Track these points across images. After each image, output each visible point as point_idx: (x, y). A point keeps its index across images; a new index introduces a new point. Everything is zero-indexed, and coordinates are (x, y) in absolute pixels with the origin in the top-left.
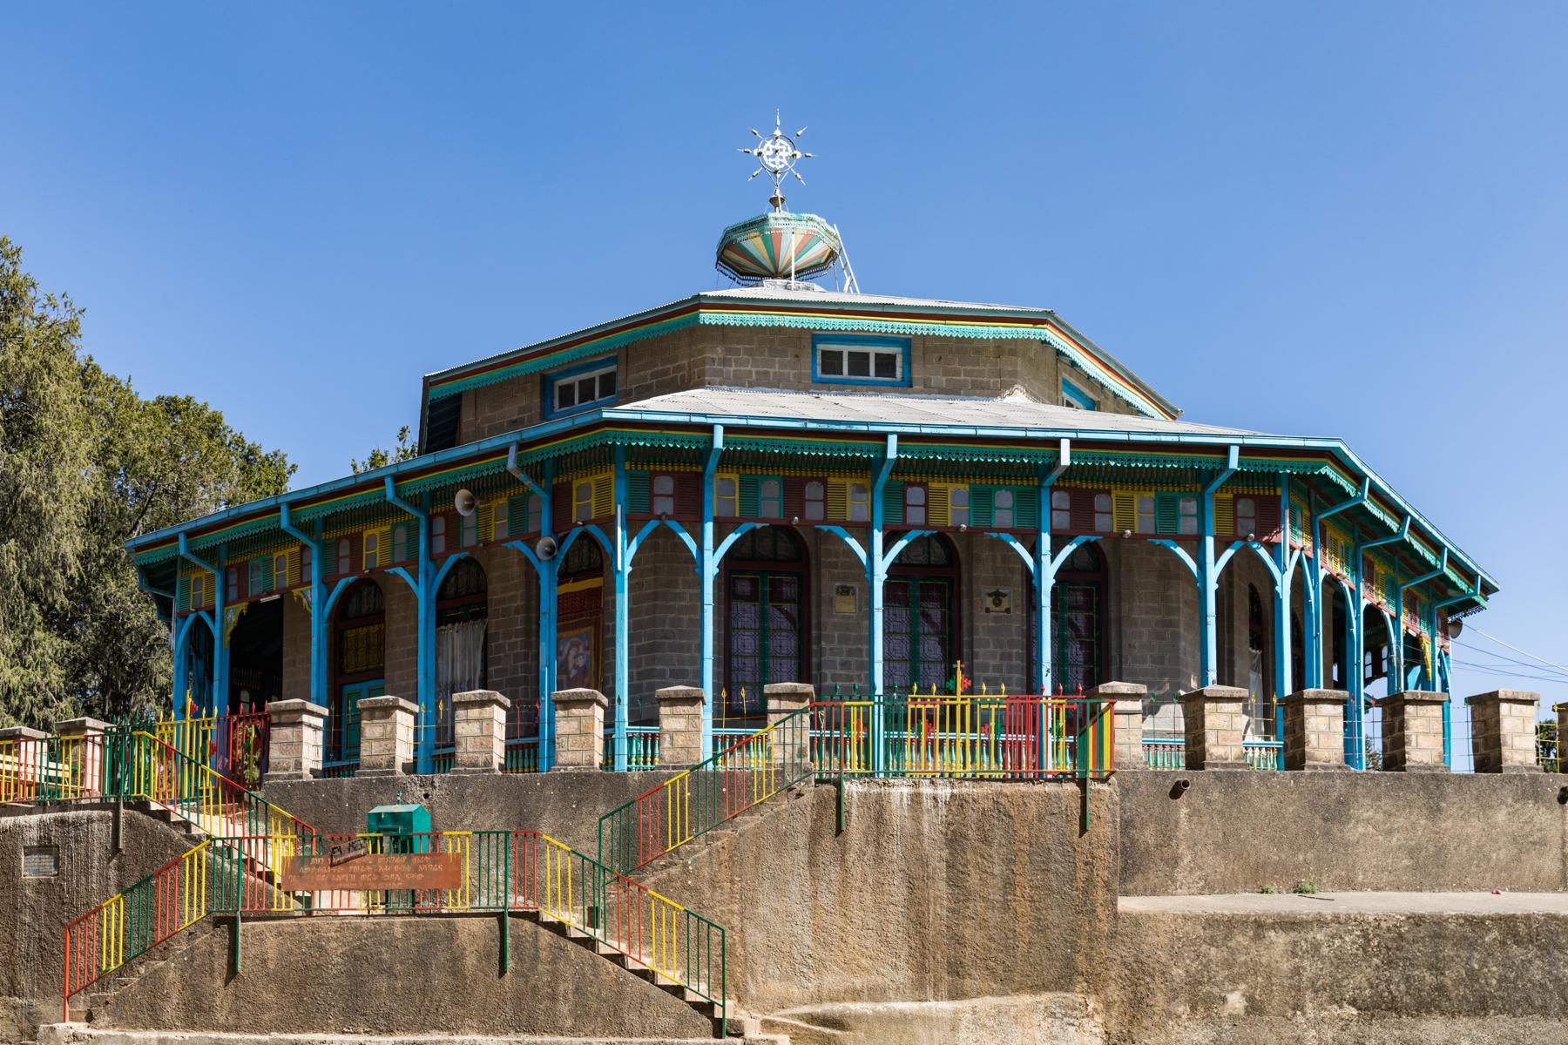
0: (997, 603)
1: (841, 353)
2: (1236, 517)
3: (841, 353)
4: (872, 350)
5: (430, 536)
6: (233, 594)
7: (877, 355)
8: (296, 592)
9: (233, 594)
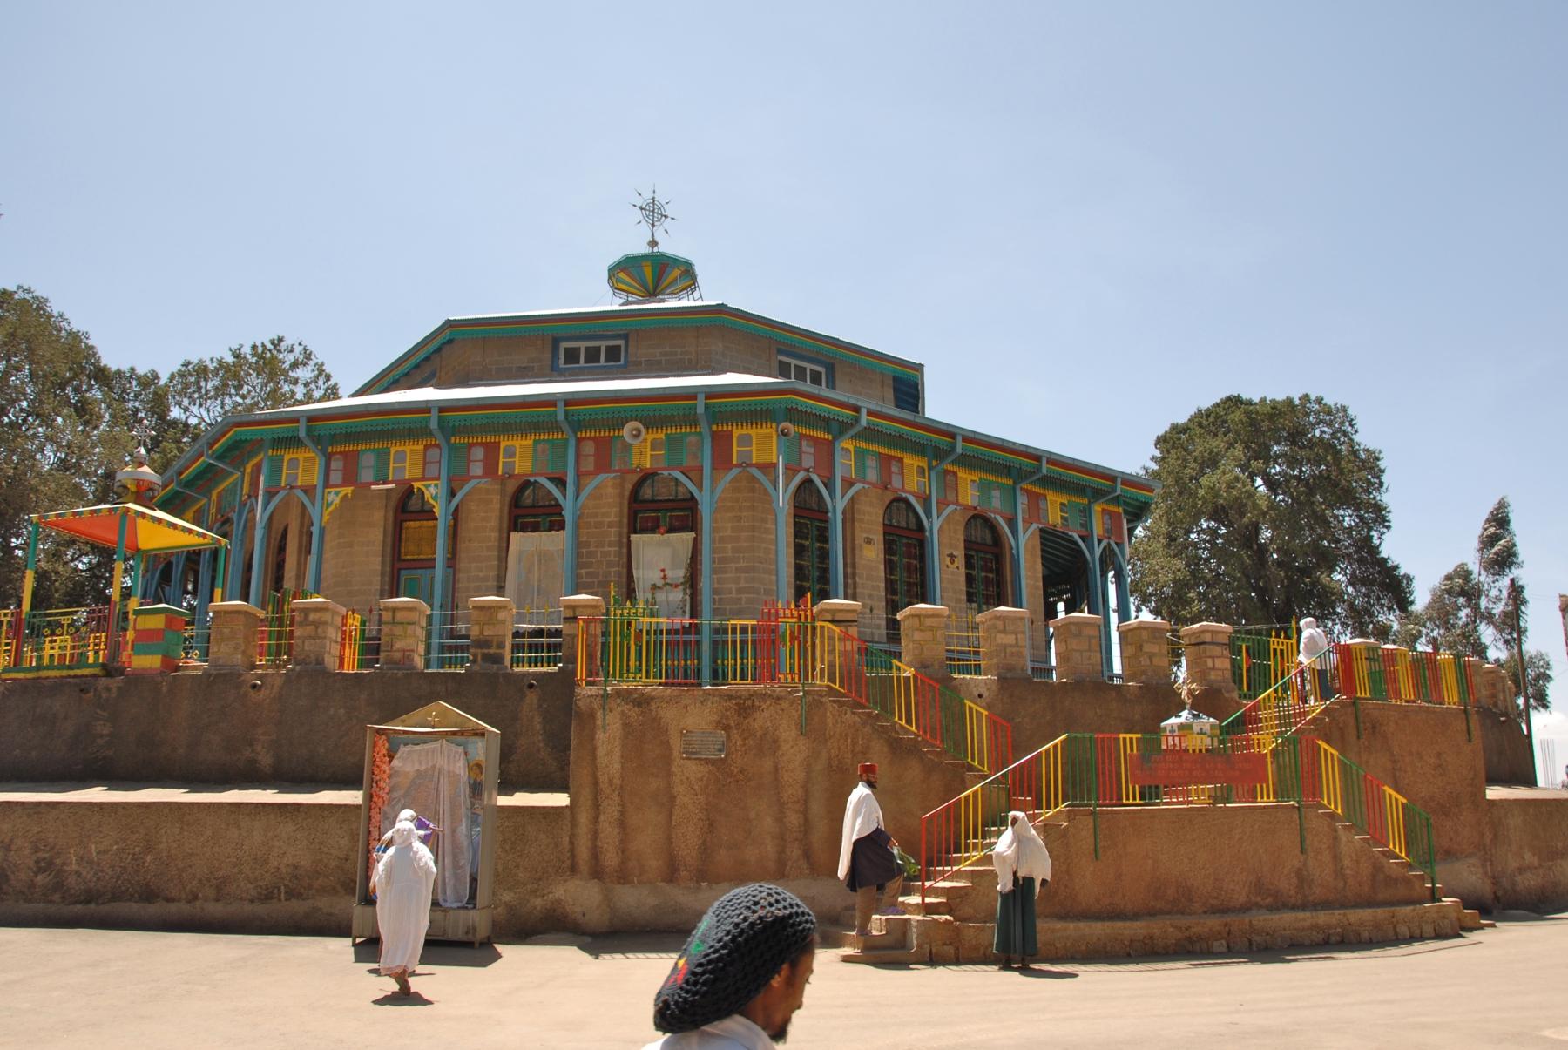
0: (952, 562)
1: (599, 348)
2: (425, 463)
3: (599, 348)
4: (603, 344)
5: (578, 455)
6: (336, 477)
7: (587, 349)
8: (416, 485)
9: (336, 477)
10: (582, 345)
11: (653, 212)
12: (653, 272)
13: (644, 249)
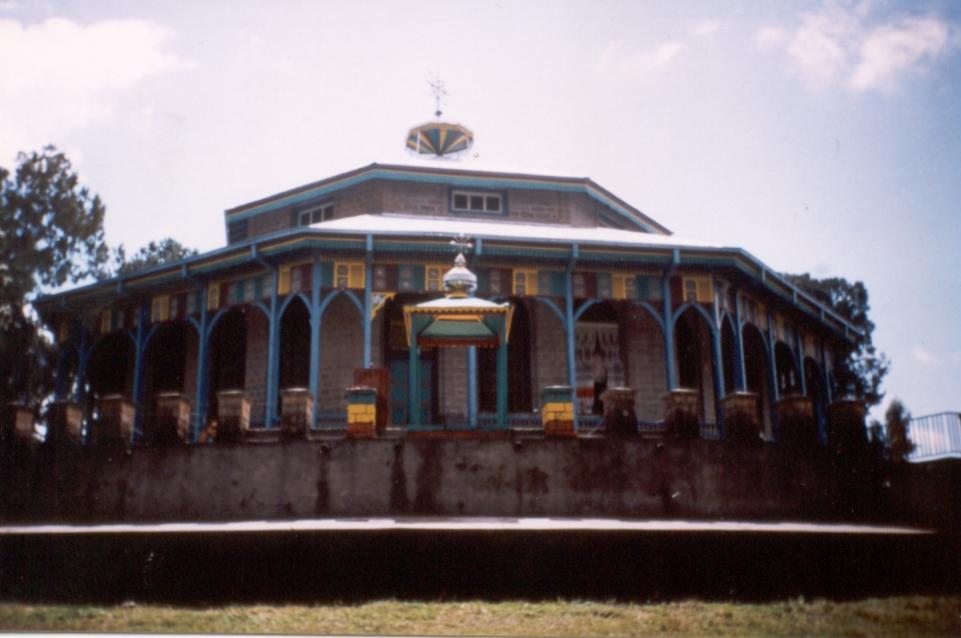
4: (485, 196)
10: (469, 194)
11: (438, 89)
12: (438, 138)
13: (434, 119)
